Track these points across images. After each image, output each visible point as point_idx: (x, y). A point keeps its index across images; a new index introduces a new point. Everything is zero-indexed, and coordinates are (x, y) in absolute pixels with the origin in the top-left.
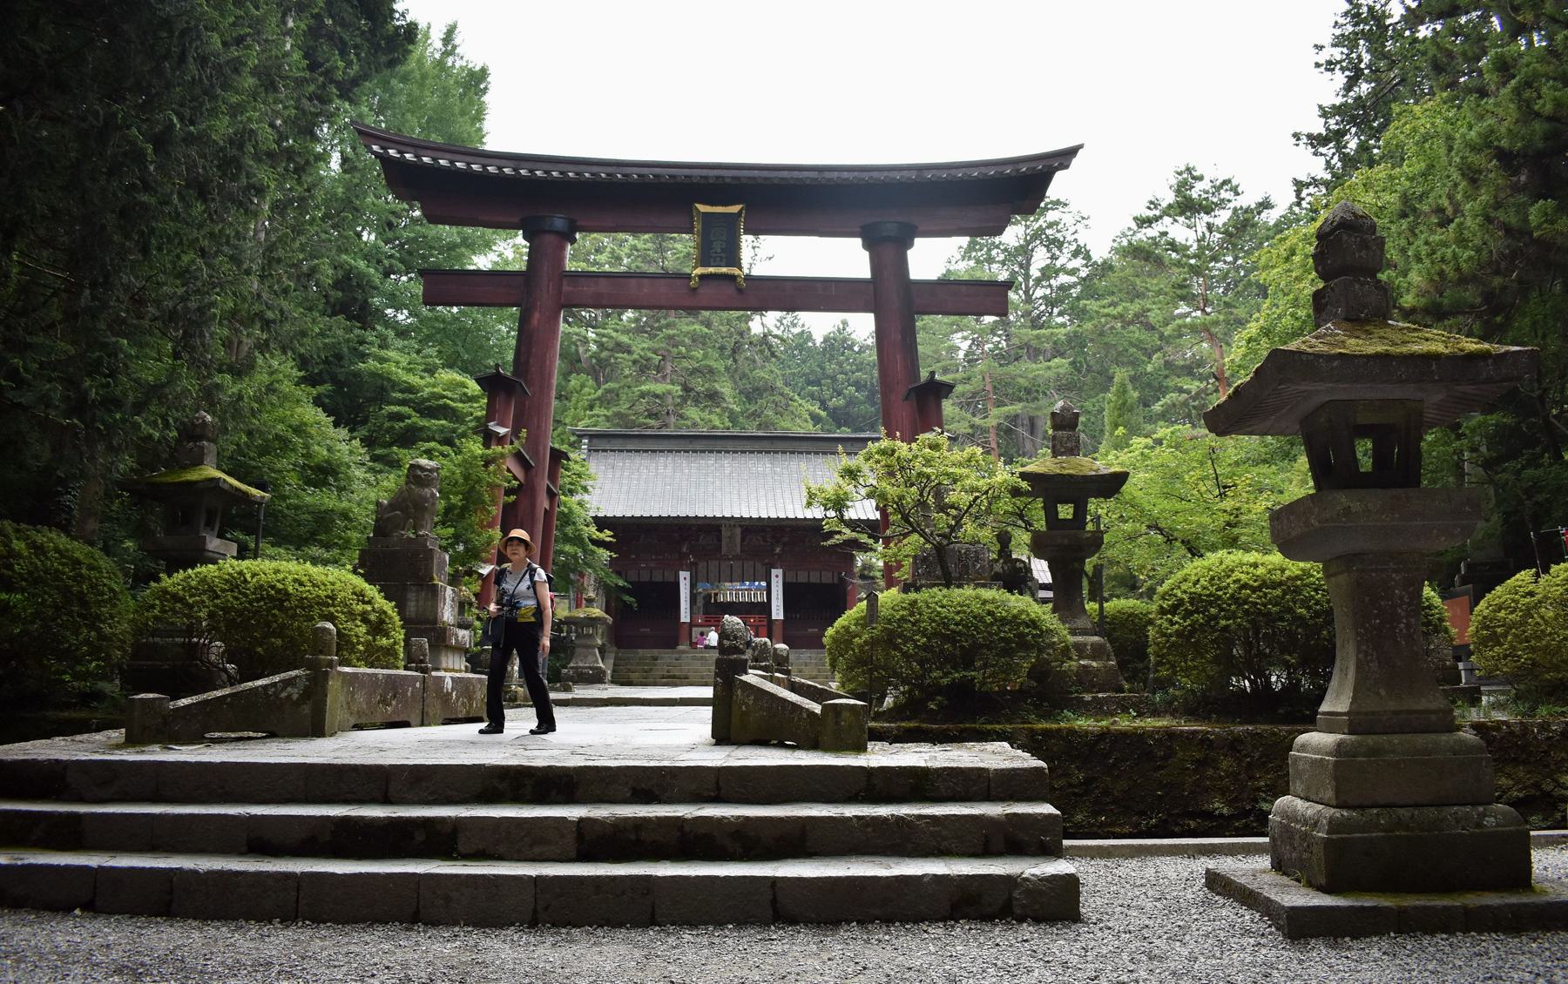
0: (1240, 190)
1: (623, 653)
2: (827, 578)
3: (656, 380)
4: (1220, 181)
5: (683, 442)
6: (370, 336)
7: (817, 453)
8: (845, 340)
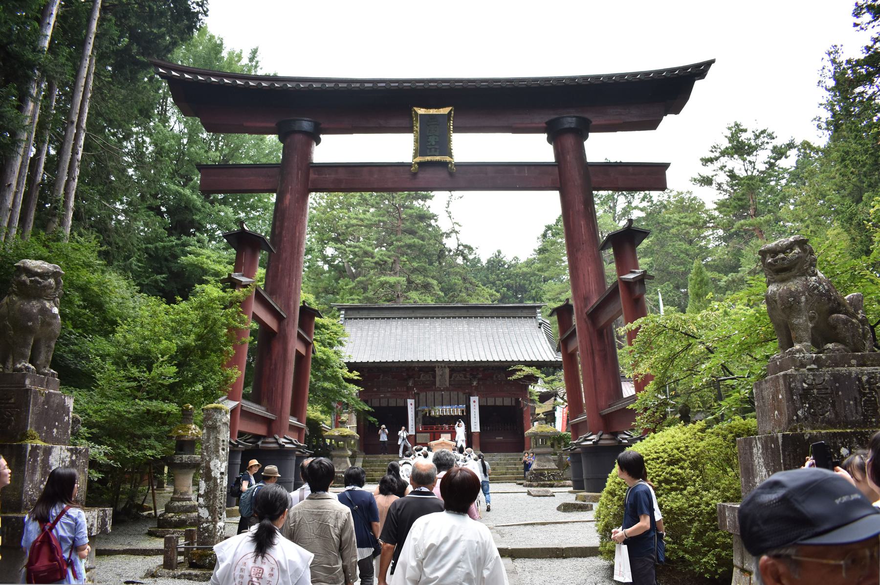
0: (774, 135)
1: (371, 458)
2: (508, 402)
3: (390, 275)
4: (759, 131)
5: (408, 311)
6: (193, 240)
7: (498, 317)
8: (500, 261)
